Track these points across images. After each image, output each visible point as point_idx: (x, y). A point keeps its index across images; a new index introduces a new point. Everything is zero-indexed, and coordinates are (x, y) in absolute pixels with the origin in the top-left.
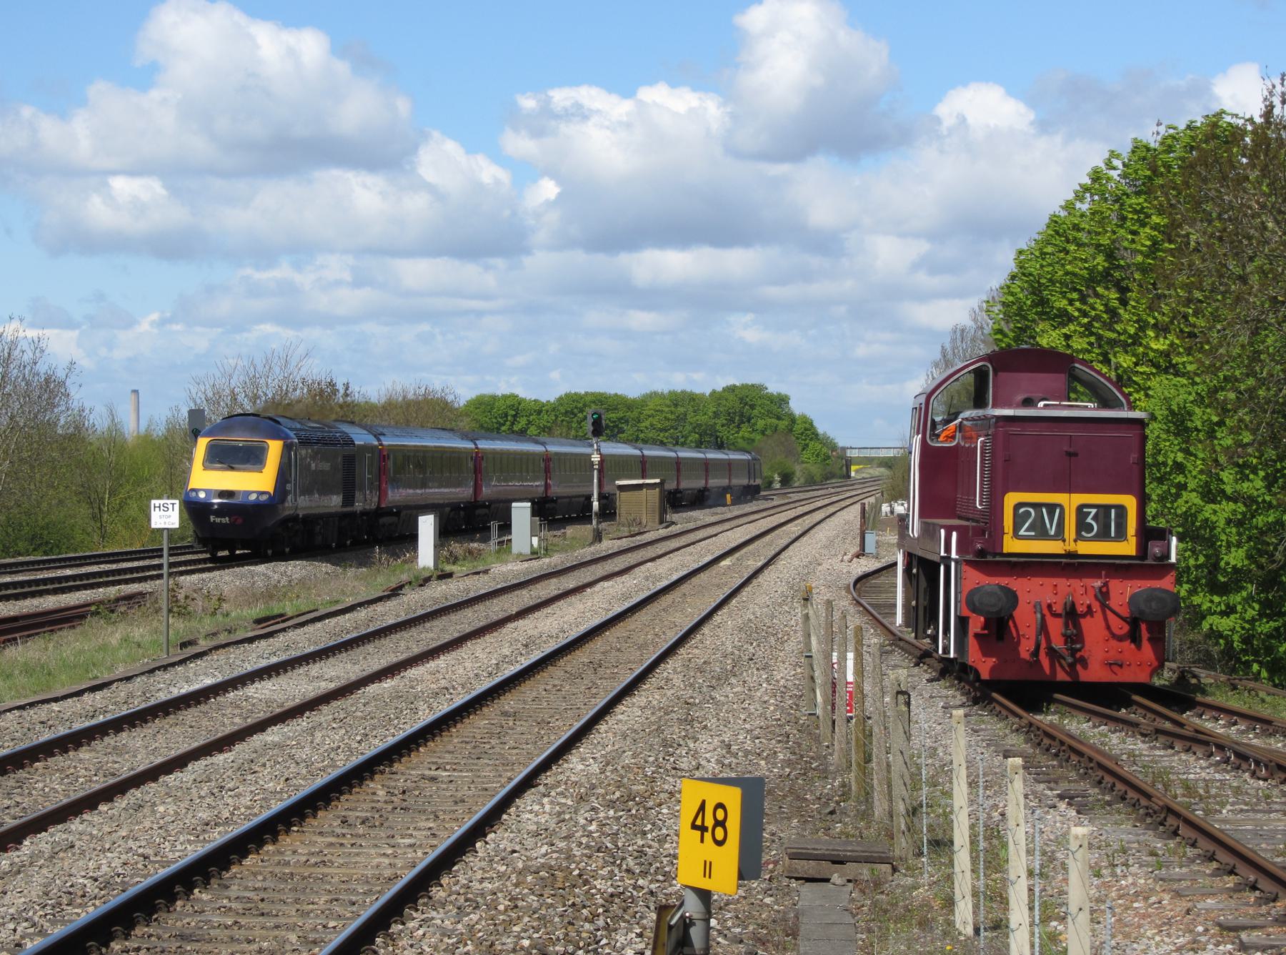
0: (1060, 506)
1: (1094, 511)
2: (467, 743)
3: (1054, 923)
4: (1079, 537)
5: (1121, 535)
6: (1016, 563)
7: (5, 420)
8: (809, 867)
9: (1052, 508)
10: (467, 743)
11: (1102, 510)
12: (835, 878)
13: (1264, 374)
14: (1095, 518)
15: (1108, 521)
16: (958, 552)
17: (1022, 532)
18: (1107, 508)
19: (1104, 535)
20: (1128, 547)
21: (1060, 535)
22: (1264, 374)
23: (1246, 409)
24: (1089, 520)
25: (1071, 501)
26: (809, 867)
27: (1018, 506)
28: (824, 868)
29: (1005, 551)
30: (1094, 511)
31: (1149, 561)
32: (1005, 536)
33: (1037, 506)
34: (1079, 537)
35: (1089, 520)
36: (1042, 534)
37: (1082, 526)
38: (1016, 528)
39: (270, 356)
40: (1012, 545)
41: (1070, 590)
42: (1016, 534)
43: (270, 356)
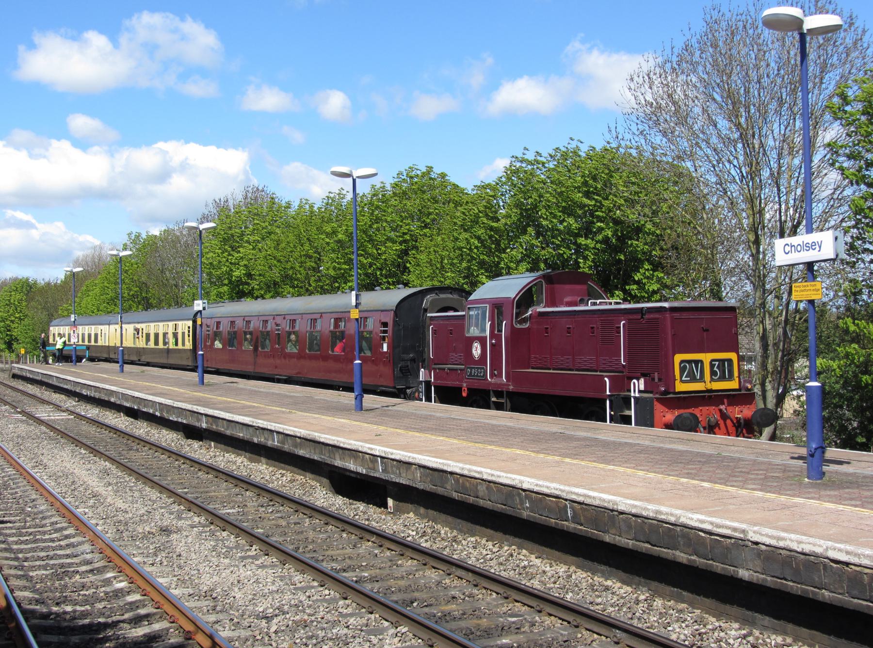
0: (702, 362)
1: (717, 363)
2: (748, 144)
3: (824, 591)
4: (712, 380)
5: (731, 377)
6: (684, 398)
7: (302, 646)
9: (697, 362)
10: (748, 144)
11: (721, 362)
14: (718, 367)
15: (723, 370)
17: (684, 378)
18: (722, 361)
19: (722, 378)
20: (733, 385)
21: (702, 379)
24: (715, 369)
25: (706, 358)
27: (682, 362)
29: (677, 391)
30: (717, 363)
31: (743, 392)
32: (676, 382)
33: (689, 362)
34: (712, 380)
35: (715, 369)
36: (693, 379)
37: (713, 373)
38: (681, 377)
39: (218, 201)
40: (680, 387)
41: (708, 412)
42: (682, 381)
43: (218, 201)
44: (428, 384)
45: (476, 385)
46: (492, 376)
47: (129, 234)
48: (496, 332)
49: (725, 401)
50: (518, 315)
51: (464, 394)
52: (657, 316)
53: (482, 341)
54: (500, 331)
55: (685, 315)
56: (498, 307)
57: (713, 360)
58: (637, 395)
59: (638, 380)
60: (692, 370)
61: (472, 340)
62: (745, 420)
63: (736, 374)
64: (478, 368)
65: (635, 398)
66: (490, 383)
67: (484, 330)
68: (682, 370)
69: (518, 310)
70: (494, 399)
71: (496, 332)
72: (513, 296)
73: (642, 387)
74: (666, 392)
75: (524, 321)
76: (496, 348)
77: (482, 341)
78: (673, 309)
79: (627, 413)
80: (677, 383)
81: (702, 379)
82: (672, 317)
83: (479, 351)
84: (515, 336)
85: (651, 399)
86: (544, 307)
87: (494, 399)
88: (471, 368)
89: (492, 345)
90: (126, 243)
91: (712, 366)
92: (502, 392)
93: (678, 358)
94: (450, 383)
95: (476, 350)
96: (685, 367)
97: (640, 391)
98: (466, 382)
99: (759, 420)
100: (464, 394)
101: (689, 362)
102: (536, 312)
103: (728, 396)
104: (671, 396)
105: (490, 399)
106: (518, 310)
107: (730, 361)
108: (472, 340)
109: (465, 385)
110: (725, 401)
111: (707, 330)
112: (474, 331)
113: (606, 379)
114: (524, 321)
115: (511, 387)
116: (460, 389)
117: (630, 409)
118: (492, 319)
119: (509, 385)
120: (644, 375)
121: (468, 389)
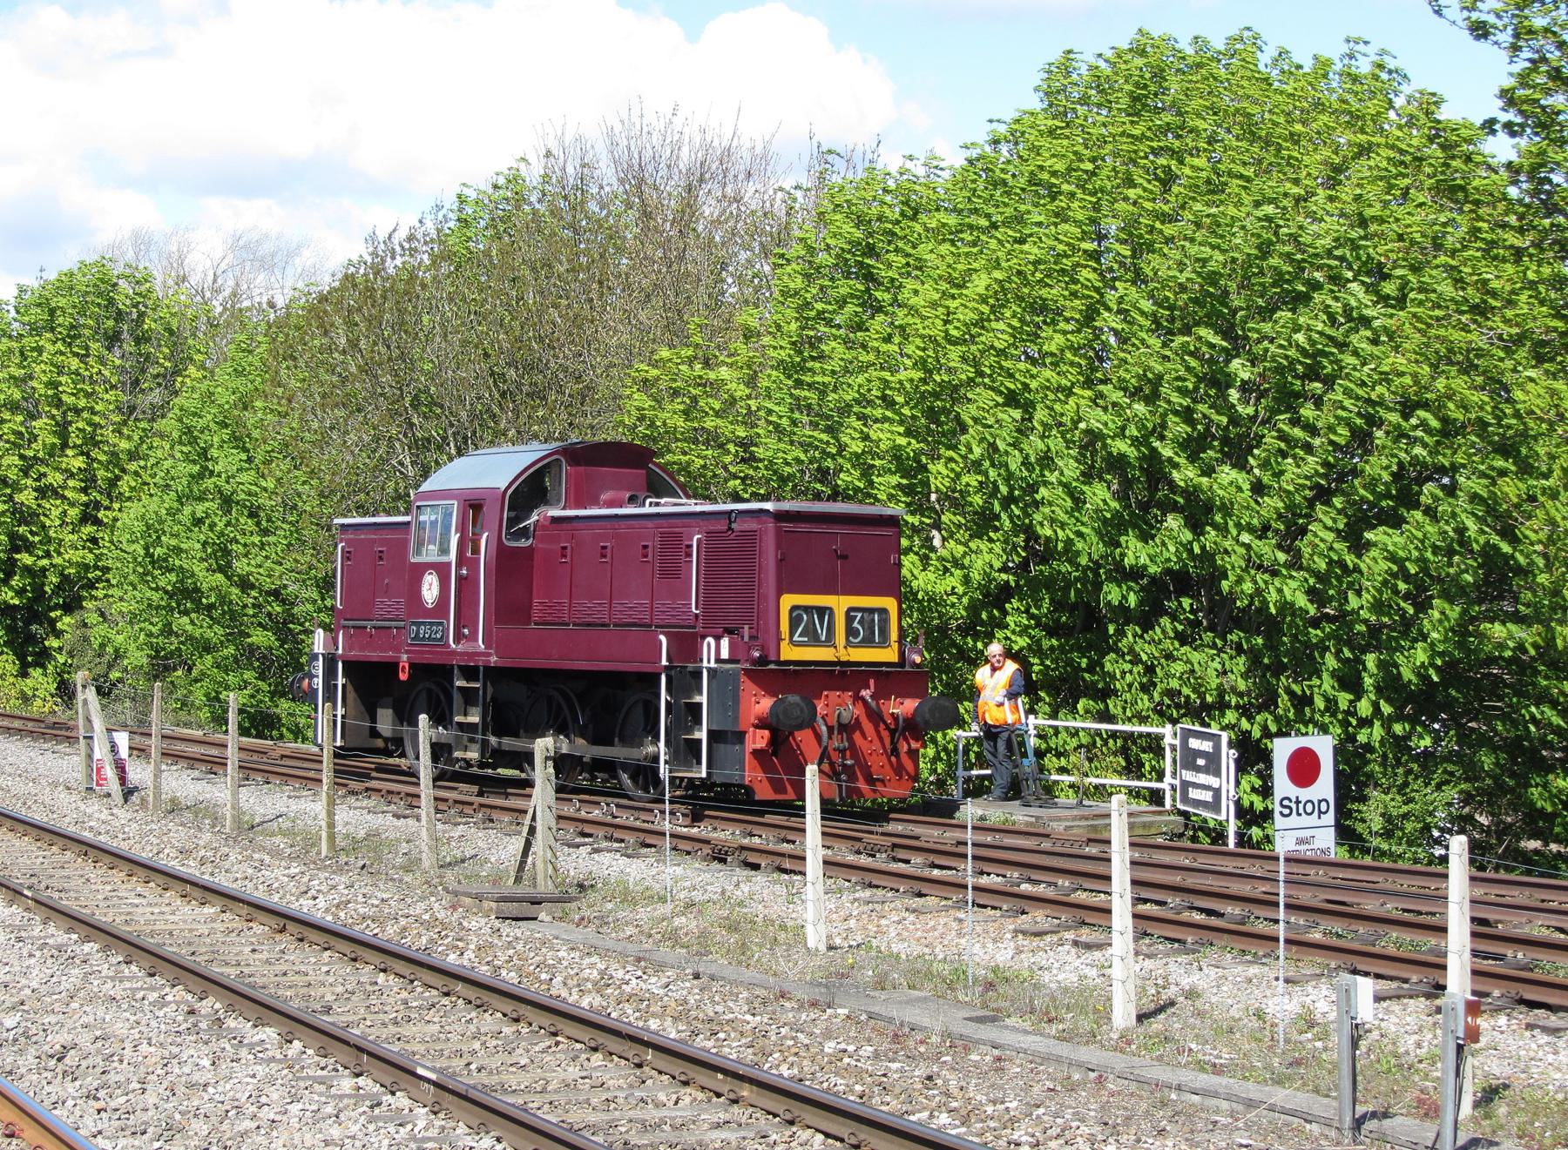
0: (830, 609)
5: (884, 642)
8: (513, 909)
9: (822, 611)
12: (542, 916)
13: (168, 364)
15: (868, 628)
16: (669, 659)
17: (796, 638)
19: (868, 642)
20: (889, 655)
21: (830, 641)
22: (168, 364)
23: (904, 482)
24: (856, 624)
25: (840, 604)
26: (513, 909)
27: (794, 608)
28: (527, 909)
31: (908, 669)
33: (807, 609)
34: (848, 644)
35: (856, 624)
36: (815, 640)
37: (851, 632)
38: (792, 634)
40: (789, 653)
43: (625, 117)
44: (330, 661)
45: (428, 658)
46: (457, 639)
47: (373, 237)
48: (469, 554)
49: (872, 682)
50: (512, 522)
51: (403, 677)
52: (754, 525)
53: (442, 570)
54: (476, 551)
55: (803, 527)
56: (474, 505)
57: (851, 609)
58: (713, 665)
59: (718, 638)
60: (811, 623)
61: (422, 569)
62: (906, 720)
63: (894, 635)
64: (431, 624)
65: (709, 670)
66: (454, 653)
67: (444, 550)
68: (794, 623)
69: (513, 514)
70: (459, 683)
71: (469, 554)
72: (503, 486)
73: (725, 654)
74: (763, 660)
75: (524, 533)
76: (466, 586)
77: (442, 570)
78: (780, 516)
79: (697, 699)
80: (784, 645)
81: (830, 641)
82: (778, 531)
83: (435, 591)
84: (510, 564)
85: (735, 673)
86: (564, 508)
87: (459, 683)
88: (418, 624)
89: (460, 578)
90: (1328, 63)
91: (849, 619)
92: (476, 668)
93: (788, 601)
94: (374, 655)
95: (430, 589)
96: (800, 618)
97: (718, 660)
98: (407, 652)
99: (927, 716)
100: (403, 677)
101: (807, 609)
102: (546, 518)
103: (878, 676)
104: (772, 666)
105: (452, 683)
106: (513, 514)
107: (883, 612)
108: (422, 569)
109: (405, 657)
110: (872, 682)
111: (844, 557)
112: (430, 554)
113: (663, 638)
114: (524, 533)
115: (494, 659)
116: (393, 667)
117: (701, 693)
118: (462, 529)
119: (489, 655)
120: (729, 632)
121: (411, 665)
